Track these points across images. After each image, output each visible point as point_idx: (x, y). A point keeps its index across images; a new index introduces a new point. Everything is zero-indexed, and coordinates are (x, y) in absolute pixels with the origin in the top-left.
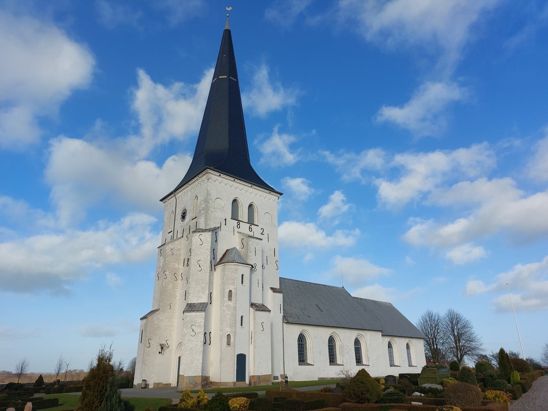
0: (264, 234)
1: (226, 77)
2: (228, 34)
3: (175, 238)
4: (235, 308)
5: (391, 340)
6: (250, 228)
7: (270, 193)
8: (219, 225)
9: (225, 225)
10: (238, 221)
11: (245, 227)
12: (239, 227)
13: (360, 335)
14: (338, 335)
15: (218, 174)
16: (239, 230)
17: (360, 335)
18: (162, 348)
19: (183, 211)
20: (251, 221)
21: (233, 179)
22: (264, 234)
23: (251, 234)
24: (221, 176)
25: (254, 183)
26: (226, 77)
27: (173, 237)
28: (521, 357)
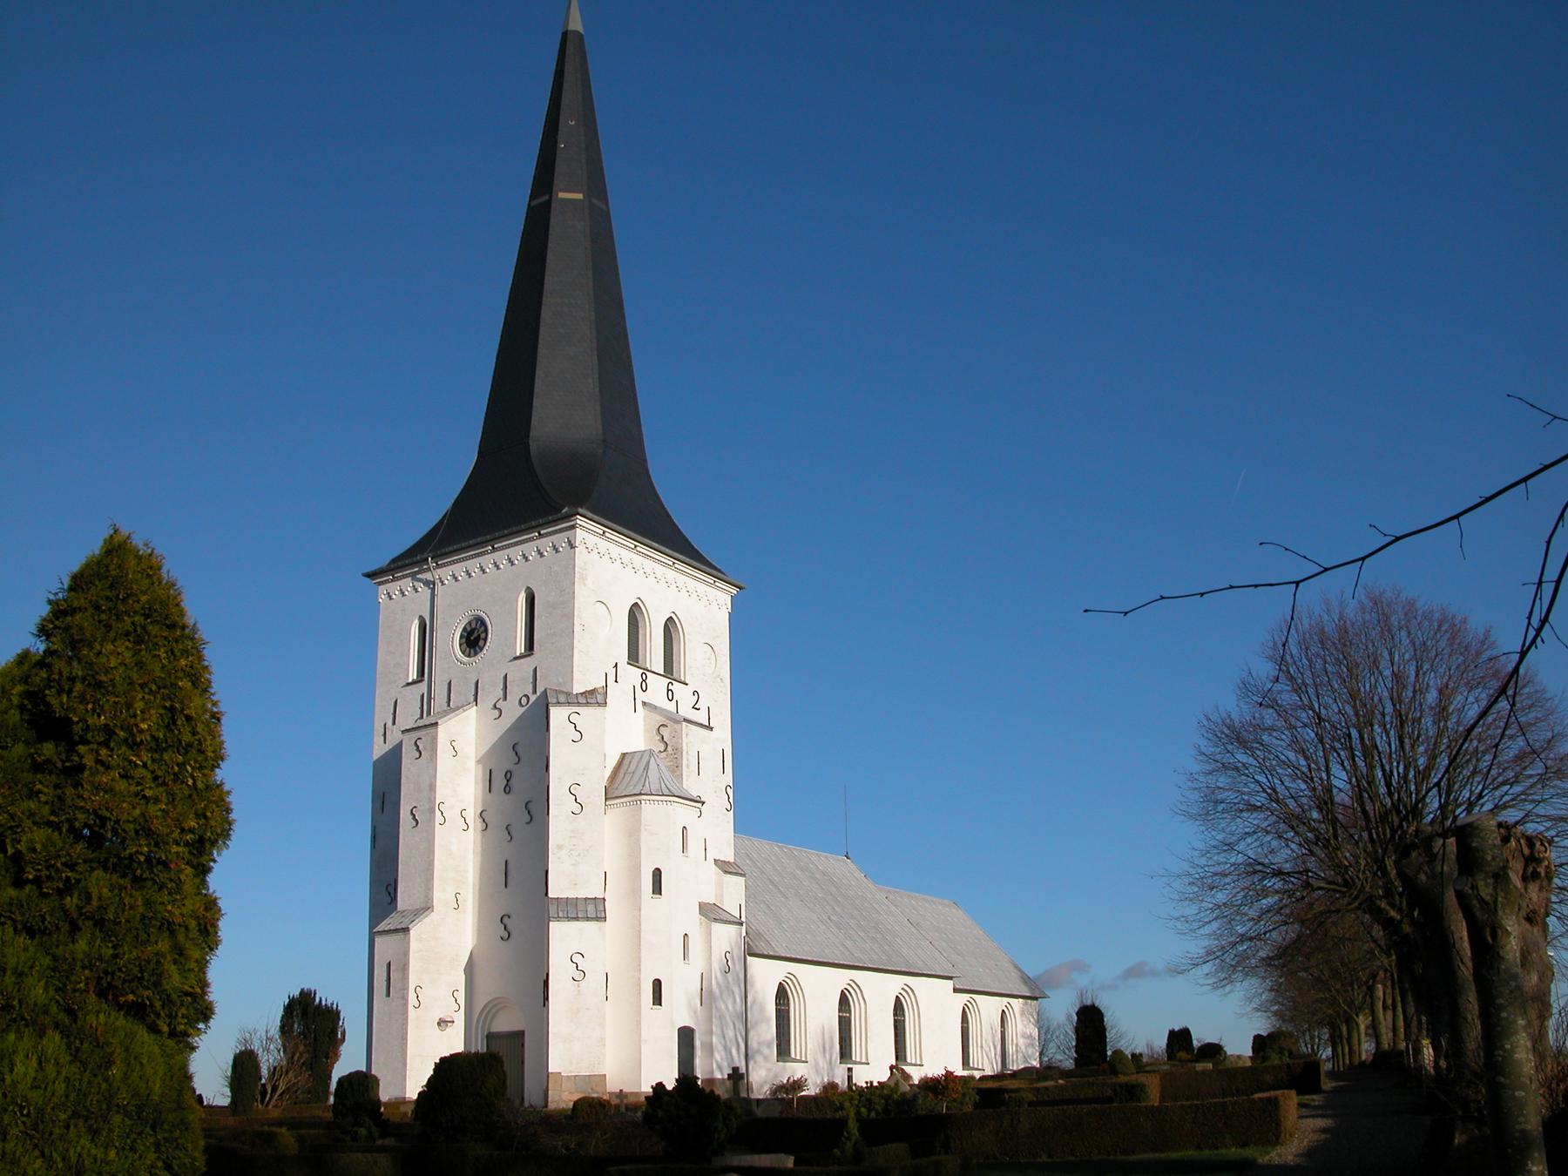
0: (698, 709)
1: (580, 196)
2: (569, 47)
5: (786, 979)
6: (668, 690)
7: (636, 546)
8: (601, 683)
9: (616, 681)
10: (643, 671)
11: (658, 684)
12: (644, 689)
13: (973, 1002)
14: (979, 1011)
15: (599, 529)
17: (973, 1002)
19: (470, 623)
20: (669, 669)
21: (669, 561)
22: (698, 709)
23: (671, 706)
24: (607, 534)
25: (681, 557)
26: (580, 196)
28: (1176, 1030)
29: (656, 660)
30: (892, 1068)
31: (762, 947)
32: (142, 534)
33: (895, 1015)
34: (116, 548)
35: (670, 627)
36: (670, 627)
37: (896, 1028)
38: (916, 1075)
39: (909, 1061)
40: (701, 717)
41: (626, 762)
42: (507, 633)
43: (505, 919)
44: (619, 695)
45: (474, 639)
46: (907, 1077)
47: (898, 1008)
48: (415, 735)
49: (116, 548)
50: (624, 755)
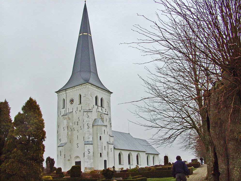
3: (67, 112)
4: (102, 143)
11: (100, 108)
19: (71, 99)
23: (102, 111)
27: (66, 111)
29: (100, 104)
30: (136, 166)
31: (116, 148)
32: (34, 98)
33: (137, 157)
34: (31, 99)
35: (102, 100)
36: (102, 100)
37: (137, 159)
38: (140, 167)
39: (139, 164)
40: (106, 113)
42: (77, 100)
43: (78, 147)
44: (94, 110)
45: (72, 101)
46: (138, 167)
47: (137, 157)
48: (63, 116)
49: (31, 99)
50: (95, 119)
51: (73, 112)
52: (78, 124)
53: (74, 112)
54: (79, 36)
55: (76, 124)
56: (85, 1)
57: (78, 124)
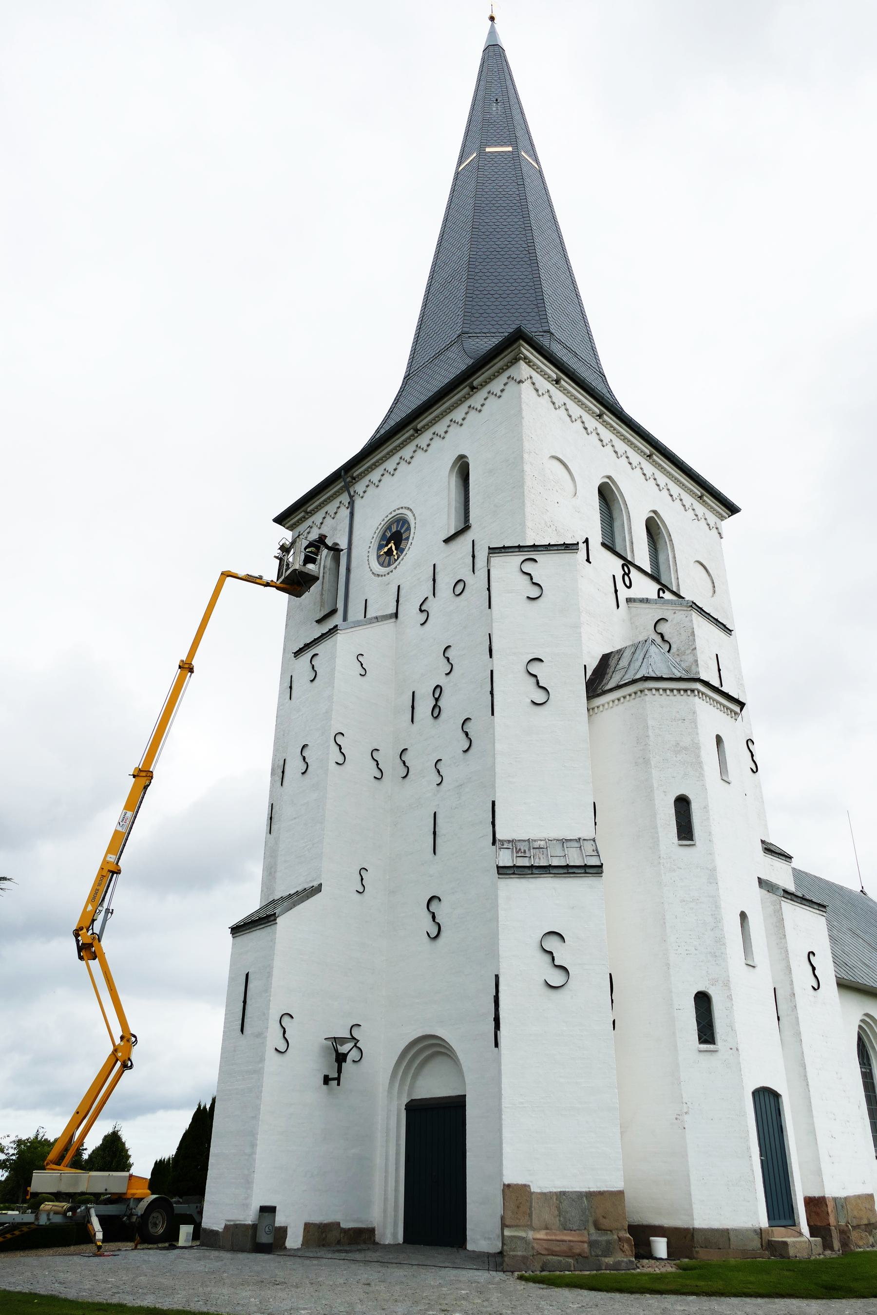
9: (588, 560)
16: (632, 593)
18: (341, 1058)
41: (613, 662)
51: (396, 615)
52: (436, 711)
53: (409, 609)
54: (457, 174)
55: (425, 706)
56: (492, 19)
57: (436, 711)
